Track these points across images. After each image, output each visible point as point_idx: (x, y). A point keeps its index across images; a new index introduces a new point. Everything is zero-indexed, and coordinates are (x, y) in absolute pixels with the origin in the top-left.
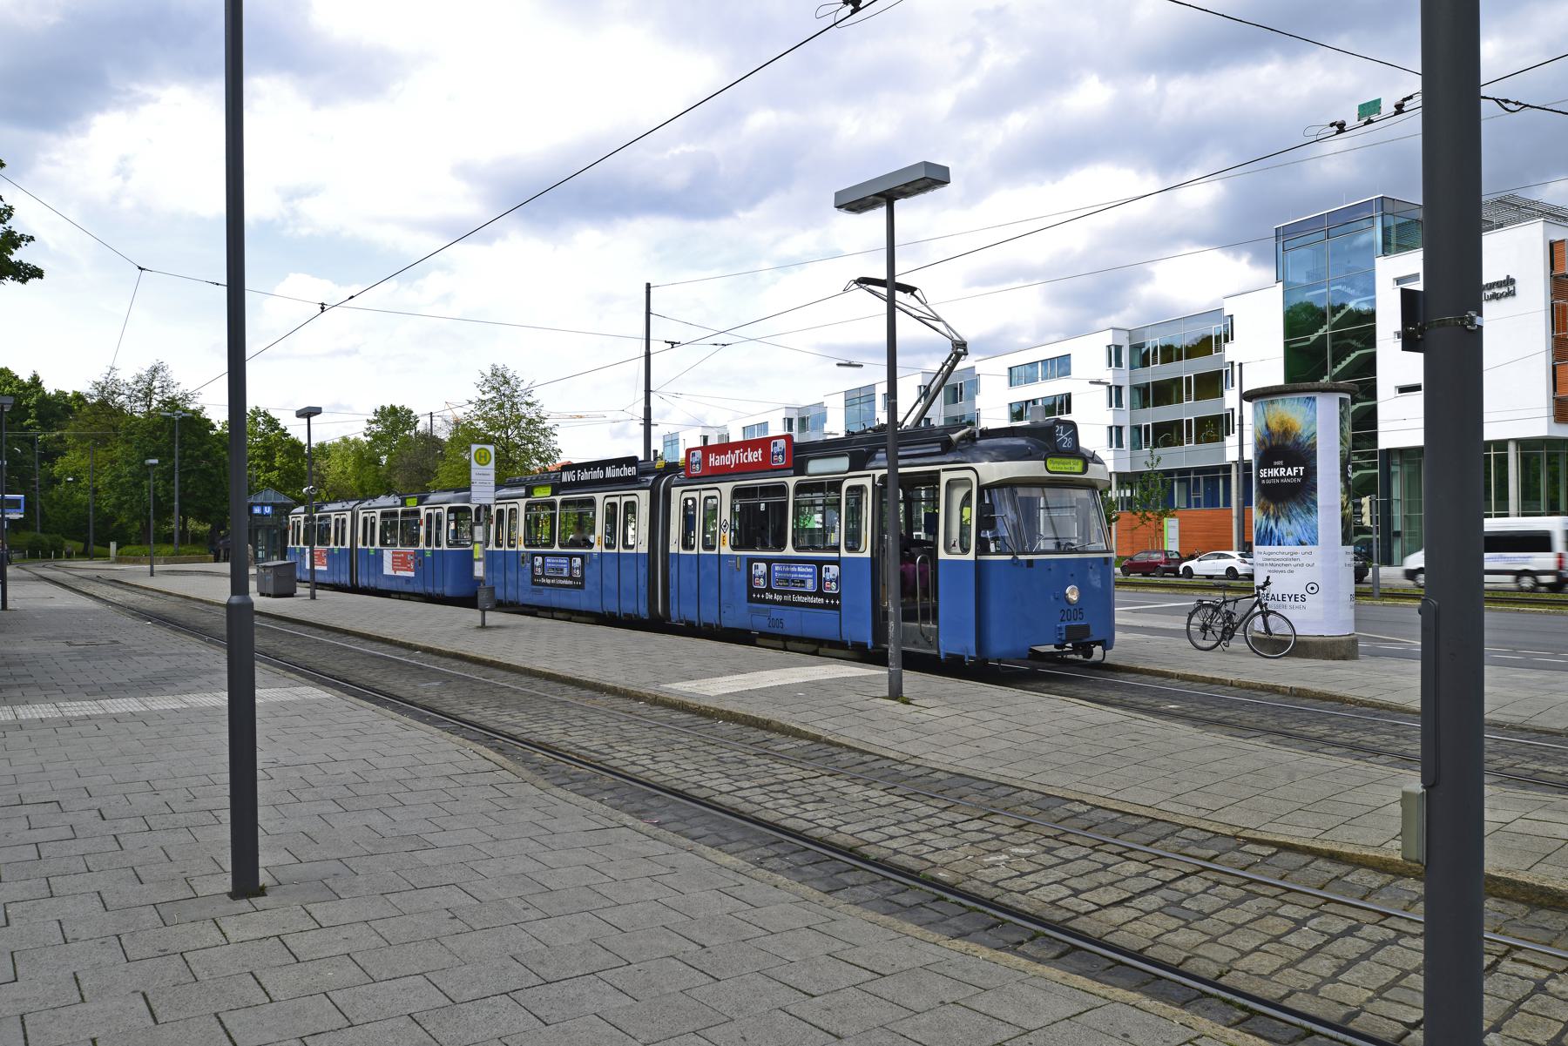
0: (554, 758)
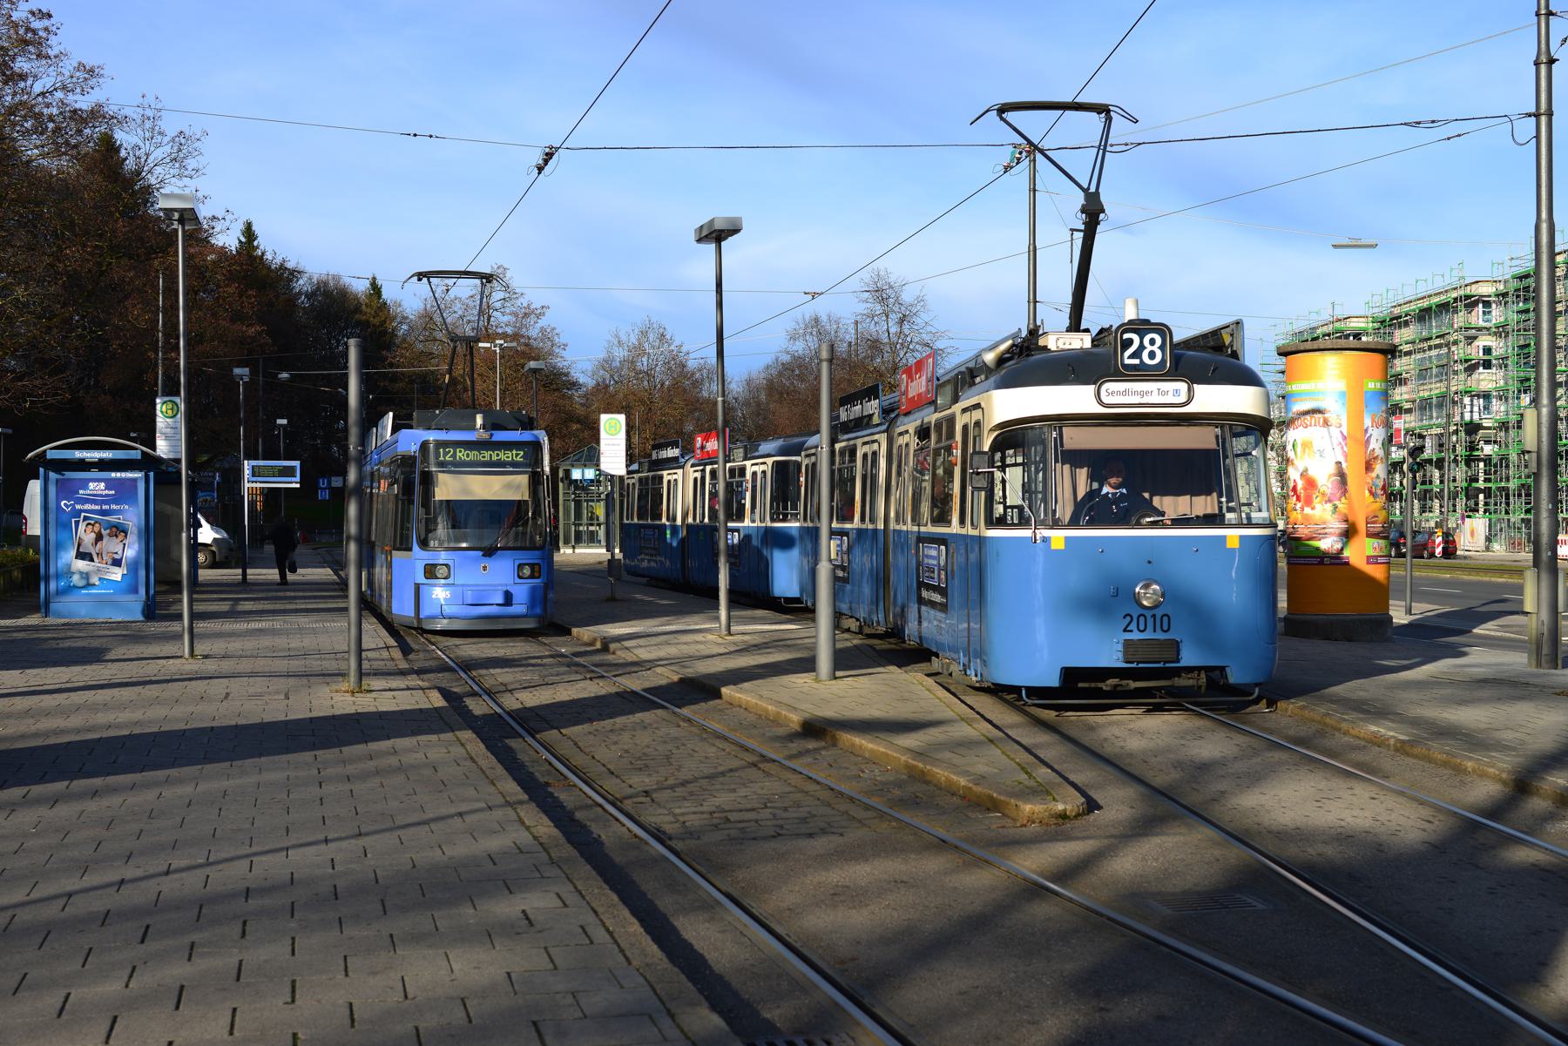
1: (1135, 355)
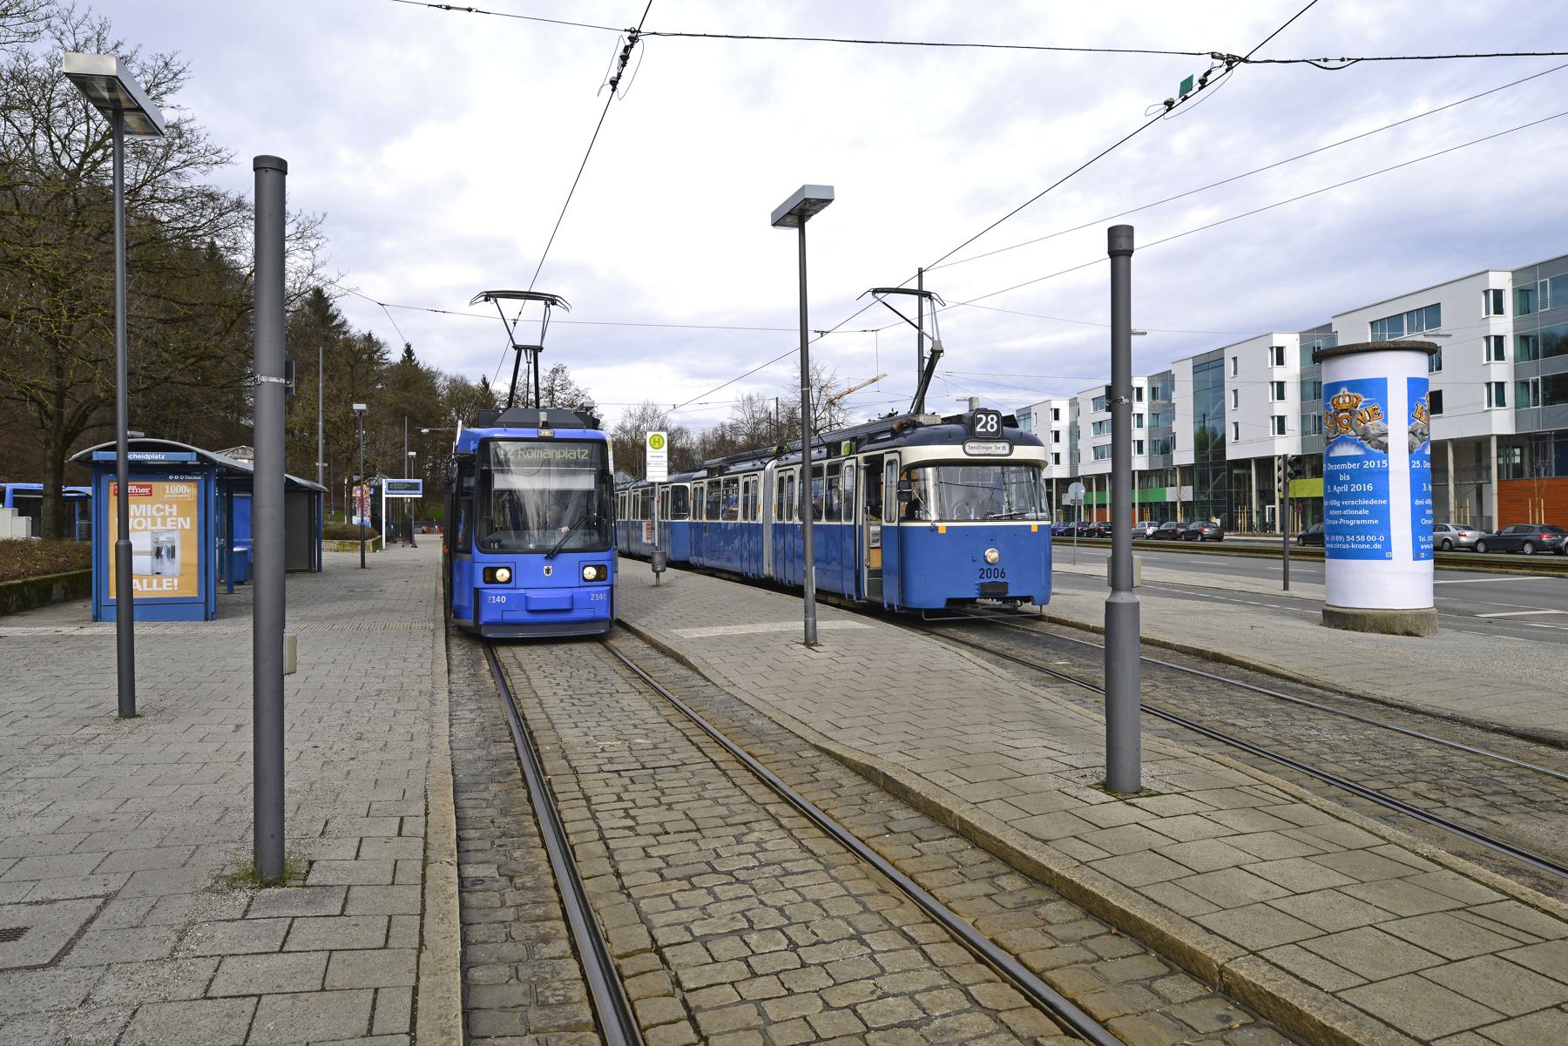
0: (1533, 770)
1: (984, 426)
